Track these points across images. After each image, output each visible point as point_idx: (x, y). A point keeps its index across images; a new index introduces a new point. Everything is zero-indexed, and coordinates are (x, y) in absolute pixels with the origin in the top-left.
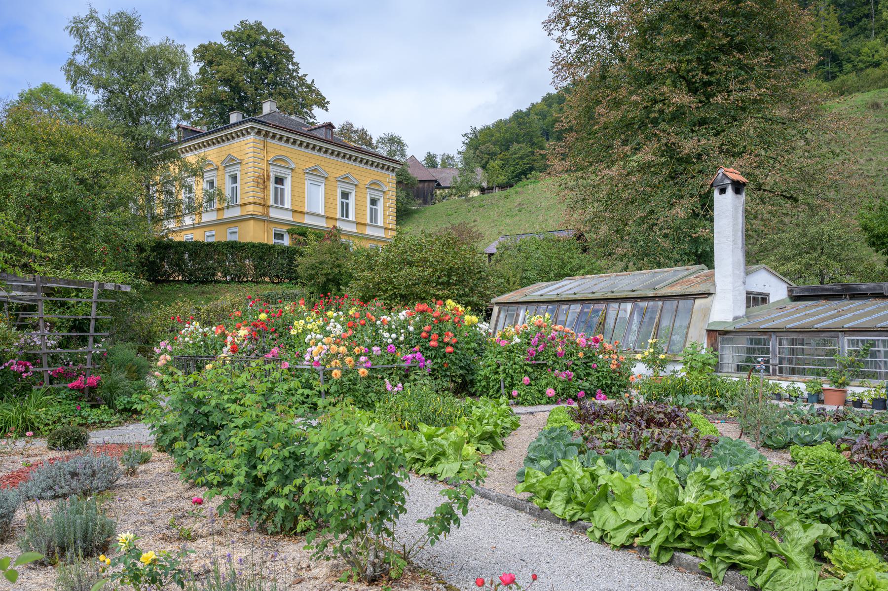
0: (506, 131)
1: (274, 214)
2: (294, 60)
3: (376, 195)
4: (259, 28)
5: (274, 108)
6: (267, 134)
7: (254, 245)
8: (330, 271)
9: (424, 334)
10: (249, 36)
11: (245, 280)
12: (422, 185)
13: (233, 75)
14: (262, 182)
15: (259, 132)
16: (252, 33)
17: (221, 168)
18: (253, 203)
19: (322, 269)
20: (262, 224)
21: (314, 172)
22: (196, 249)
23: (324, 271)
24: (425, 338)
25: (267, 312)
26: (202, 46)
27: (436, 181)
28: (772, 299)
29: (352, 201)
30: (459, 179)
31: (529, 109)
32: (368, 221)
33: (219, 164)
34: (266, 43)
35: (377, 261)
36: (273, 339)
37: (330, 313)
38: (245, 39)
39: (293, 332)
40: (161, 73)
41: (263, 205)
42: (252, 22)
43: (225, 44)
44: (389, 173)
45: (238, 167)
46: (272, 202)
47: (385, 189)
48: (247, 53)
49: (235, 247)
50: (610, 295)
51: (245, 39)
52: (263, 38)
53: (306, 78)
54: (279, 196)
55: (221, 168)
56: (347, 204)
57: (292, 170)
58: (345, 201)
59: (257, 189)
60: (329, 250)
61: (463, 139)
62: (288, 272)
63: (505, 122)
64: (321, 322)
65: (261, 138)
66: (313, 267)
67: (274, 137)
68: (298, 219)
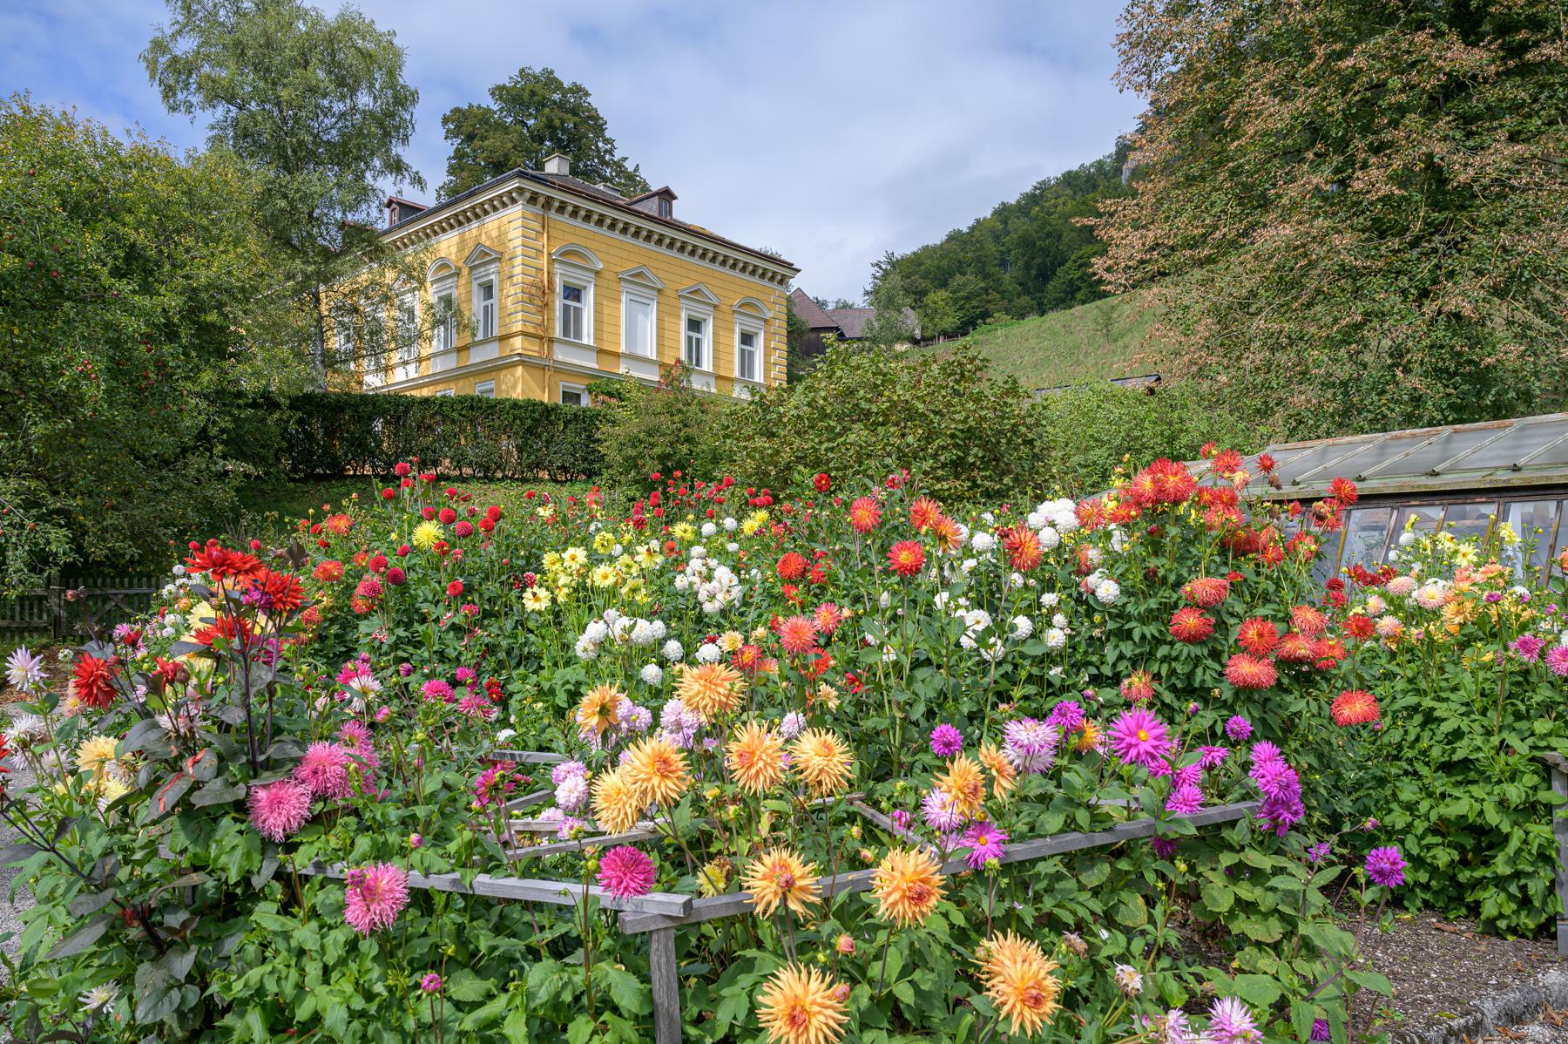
0: (942, 257)
1: (561, 355)
2: (608, 134)
3: (751, 325)
4: (550, 81)
5: (566, 170)
6: (548, 203)
7: (515, 405)
8: (668, 450)
9: (1190, 621)
10: (533, 94)
11: (499, 475)
12: (813, 336)
13: (506, 156)
14: (539, 295)
15: (533, 199)
16: (538, 88)
18: (523, 334)
19: (653, 446)
20: (539, 373)
22: (396, 408)
23: (658, 450)
24: (1193, 639)
25: (449, 520)
26: (457, 110)
27: (837, 329)
30: (876, 324)
31: (972, 229)
32: (736, 374)
33: (460, 264)
34: (561, 105)
35: (781, 416)
36: (455, 628)
37: (680, 530)
38: (526, 97)
39: (536, 601)
40: (346, 83)
41: (541, 338)
42: (537, 70)
43: (495, 108)
45: (493, 268)
46: (558, 332)
47: (769, 315)
48: (531, 122)
49: (477, 409)
50: (1504, 478)
51: (526, 97)
52: (557, 97)
53: (626, 164)
54: (571, 322)
55: (465, 271)
56: (698, 340)
57: (597, 273)
58: (695, 335)
59: (532, 308)
60: (668, 405)
61: (873, 270)
62: (584, 459)
63: (935, 249)
64: (648, 556)
65: (537, 209)
66: (635, 442)
67: (561, 209)
68: (607, 366)
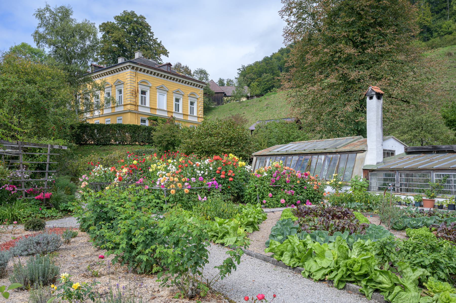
0: (260, 67)
1: (141, 110)
2: (151, 31)
3: (193, 100)
4: (133, 14)
5: (141, 55)
6: (137, 69)
7: (130, 126)
8: (169, 139)
9: (218, 171)
10: (128, 19)
11: (126, 143)
12: (216, 95)
13: (119, 39)
14: (135, 93)
15: (133, 68)
16: (129, 17)
17: (114, 86)
18: (130, 104)
19: (165, 138)
20: (134, 115)
21: (161, 88)
22: (101, 128)
23: (166, 139)
24: (218, 173)
25: (137, 160)
26: (103, 24)
27: (224, 93)
28: (396, 153)
29: (181, 103)
30: (236, 92)
31: (272, 56)
32: (189, 113)
33: (112, 84)
34: (136, 22)
35: (193, 134)
36: (140, 174)
37: (169, 161)
38: (126, 20)
39: (151, 170)
40: (83, 38)
41: (135, 105)
42: (129, 11)
43: (116, 23)
44: (200, 88)
45: (122, 86)
46: (139, 104)
47: (198, 97)
48: (127, 27)
49: (120, 127)
50: (313, 151)
51: (126, 20)
52: (135, 19)
53: (157, 40)
54: (143, 101)
55: (114, 86)
56: (178, 105)
57: (150, 87)
58: (177, 103)
59: (132, 97)
60: (169, 128)
61: (238, 71)
62: (148, 140)
63: (260, 63)
64: (165, 165)
65: (134, 71)
66: (161, 137)
67: (141, 70)
68: (153, 112)
